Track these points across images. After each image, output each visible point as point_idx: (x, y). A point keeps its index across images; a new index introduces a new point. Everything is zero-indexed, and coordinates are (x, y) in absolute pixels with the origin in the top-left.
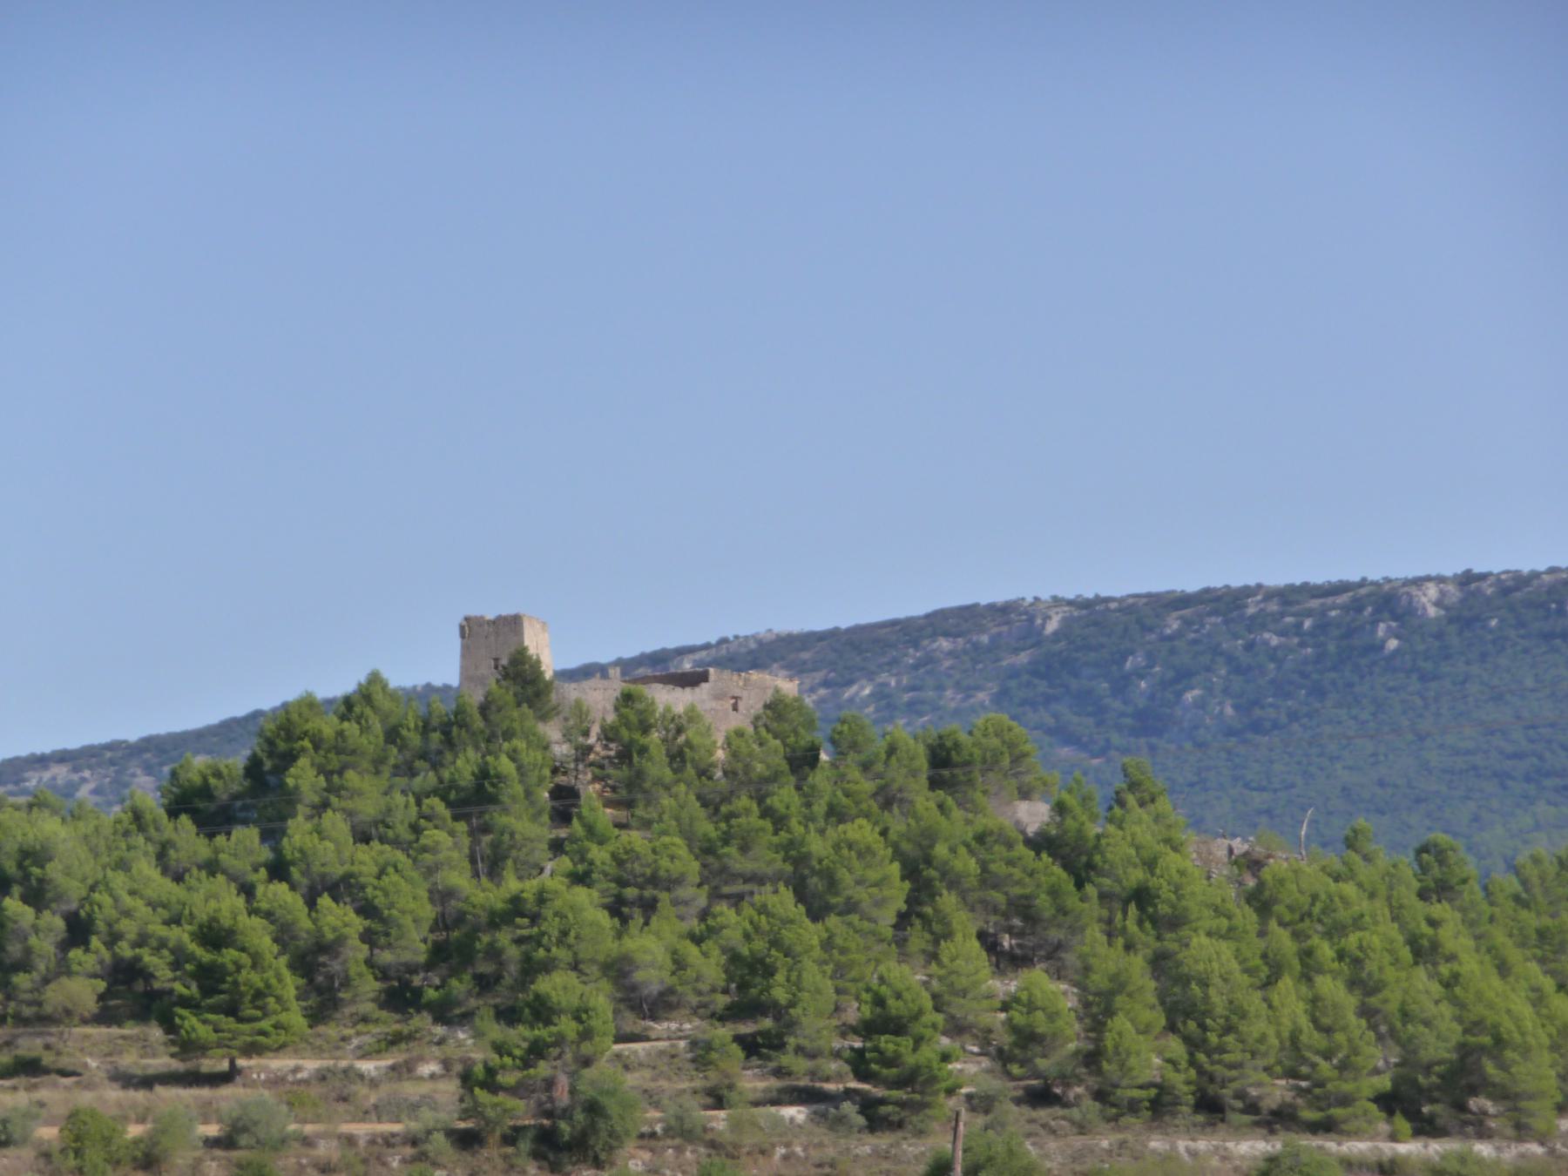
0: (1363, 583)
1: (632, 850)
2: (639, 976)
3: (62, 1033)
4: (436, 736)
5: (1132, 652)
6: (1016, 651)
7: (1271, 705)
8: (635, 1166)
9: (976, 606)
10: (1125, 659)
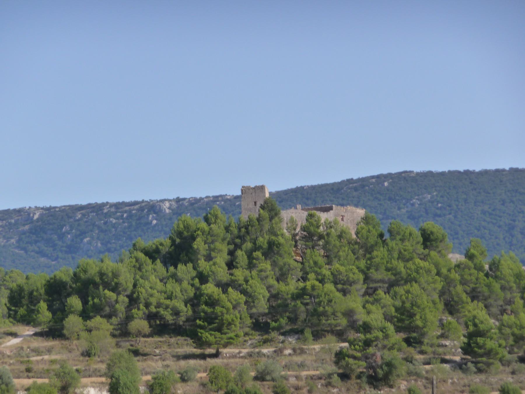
0: (143, 201)
1: (339, 270)
2: (356, 317)
3: (136, 340)
4: (243, 230)
5: (65, 225)
6: (24, 225)
7: (114, 243)
8: (403, 385)
9: (9, 210)
10: (62, 228)
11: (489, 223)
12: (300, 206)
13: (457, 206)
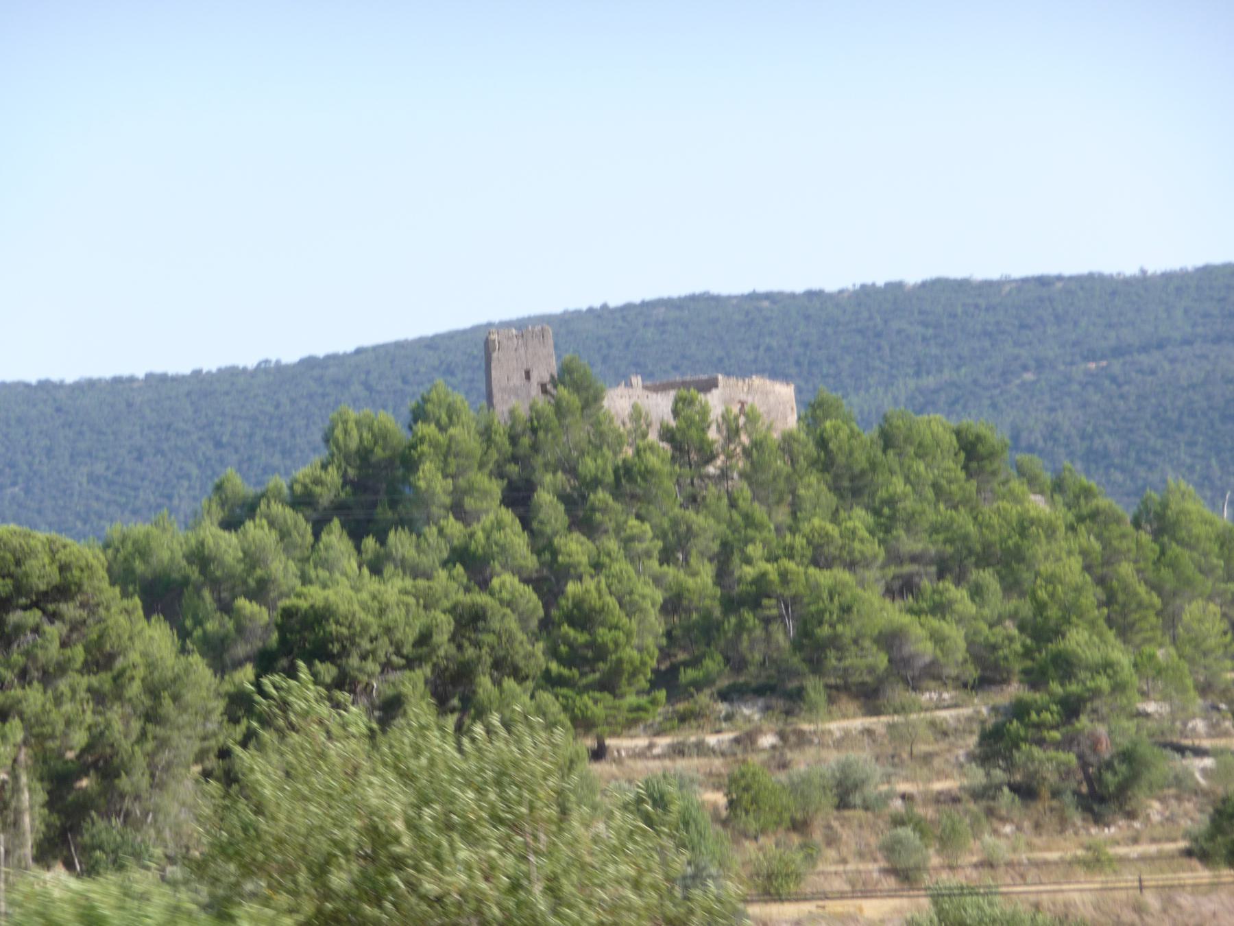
2: (909, 649)
11: (108, 503)
12: (639, 378)
13: (30, 465)
